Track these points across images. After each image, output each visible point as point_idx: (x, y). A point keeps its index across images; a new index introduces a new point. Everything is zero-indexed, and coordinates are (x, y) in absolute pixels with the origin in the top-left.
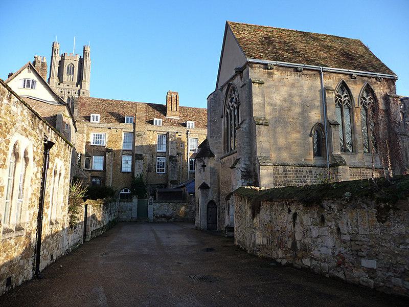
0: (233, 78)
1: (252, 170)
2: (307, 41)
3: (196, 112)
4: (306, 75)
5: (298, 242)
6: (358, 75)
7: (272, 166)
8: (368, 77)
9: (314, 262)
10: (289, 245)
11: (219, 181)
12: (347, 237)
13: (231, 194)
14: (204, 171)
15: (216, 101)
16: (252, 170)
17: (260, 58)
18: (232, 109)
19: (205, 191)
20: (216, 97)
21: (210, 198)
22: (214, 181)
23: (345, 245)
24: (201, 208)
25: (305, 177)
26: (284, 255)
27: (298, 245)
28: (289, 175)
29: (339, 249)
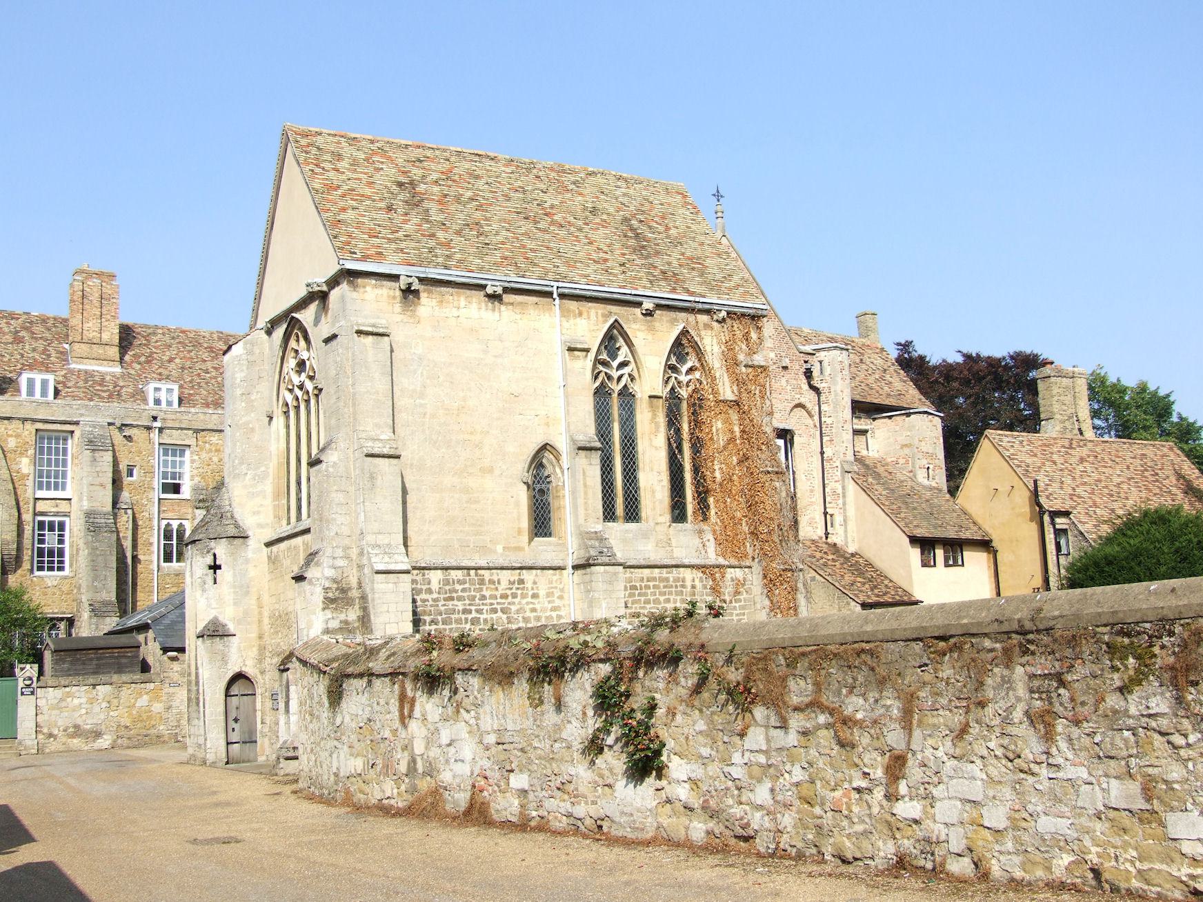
0: (302, 304)
1: (354, 582)
2: (524, 192)
3: (185, 345)
4: (512, 304)
6: (658, 306)
7: (407, 572)
8: (198, 699)
10: (403, 768)
11: (260, 613)
12: (491, 739)
14: (215, 583)
16: (354, 582)
18: (299, 393)
20: (250, 353)
22: (246, 613)
25: (504, 596)
26: (395, 791)
28: (460, 594)
29: (480, 763)
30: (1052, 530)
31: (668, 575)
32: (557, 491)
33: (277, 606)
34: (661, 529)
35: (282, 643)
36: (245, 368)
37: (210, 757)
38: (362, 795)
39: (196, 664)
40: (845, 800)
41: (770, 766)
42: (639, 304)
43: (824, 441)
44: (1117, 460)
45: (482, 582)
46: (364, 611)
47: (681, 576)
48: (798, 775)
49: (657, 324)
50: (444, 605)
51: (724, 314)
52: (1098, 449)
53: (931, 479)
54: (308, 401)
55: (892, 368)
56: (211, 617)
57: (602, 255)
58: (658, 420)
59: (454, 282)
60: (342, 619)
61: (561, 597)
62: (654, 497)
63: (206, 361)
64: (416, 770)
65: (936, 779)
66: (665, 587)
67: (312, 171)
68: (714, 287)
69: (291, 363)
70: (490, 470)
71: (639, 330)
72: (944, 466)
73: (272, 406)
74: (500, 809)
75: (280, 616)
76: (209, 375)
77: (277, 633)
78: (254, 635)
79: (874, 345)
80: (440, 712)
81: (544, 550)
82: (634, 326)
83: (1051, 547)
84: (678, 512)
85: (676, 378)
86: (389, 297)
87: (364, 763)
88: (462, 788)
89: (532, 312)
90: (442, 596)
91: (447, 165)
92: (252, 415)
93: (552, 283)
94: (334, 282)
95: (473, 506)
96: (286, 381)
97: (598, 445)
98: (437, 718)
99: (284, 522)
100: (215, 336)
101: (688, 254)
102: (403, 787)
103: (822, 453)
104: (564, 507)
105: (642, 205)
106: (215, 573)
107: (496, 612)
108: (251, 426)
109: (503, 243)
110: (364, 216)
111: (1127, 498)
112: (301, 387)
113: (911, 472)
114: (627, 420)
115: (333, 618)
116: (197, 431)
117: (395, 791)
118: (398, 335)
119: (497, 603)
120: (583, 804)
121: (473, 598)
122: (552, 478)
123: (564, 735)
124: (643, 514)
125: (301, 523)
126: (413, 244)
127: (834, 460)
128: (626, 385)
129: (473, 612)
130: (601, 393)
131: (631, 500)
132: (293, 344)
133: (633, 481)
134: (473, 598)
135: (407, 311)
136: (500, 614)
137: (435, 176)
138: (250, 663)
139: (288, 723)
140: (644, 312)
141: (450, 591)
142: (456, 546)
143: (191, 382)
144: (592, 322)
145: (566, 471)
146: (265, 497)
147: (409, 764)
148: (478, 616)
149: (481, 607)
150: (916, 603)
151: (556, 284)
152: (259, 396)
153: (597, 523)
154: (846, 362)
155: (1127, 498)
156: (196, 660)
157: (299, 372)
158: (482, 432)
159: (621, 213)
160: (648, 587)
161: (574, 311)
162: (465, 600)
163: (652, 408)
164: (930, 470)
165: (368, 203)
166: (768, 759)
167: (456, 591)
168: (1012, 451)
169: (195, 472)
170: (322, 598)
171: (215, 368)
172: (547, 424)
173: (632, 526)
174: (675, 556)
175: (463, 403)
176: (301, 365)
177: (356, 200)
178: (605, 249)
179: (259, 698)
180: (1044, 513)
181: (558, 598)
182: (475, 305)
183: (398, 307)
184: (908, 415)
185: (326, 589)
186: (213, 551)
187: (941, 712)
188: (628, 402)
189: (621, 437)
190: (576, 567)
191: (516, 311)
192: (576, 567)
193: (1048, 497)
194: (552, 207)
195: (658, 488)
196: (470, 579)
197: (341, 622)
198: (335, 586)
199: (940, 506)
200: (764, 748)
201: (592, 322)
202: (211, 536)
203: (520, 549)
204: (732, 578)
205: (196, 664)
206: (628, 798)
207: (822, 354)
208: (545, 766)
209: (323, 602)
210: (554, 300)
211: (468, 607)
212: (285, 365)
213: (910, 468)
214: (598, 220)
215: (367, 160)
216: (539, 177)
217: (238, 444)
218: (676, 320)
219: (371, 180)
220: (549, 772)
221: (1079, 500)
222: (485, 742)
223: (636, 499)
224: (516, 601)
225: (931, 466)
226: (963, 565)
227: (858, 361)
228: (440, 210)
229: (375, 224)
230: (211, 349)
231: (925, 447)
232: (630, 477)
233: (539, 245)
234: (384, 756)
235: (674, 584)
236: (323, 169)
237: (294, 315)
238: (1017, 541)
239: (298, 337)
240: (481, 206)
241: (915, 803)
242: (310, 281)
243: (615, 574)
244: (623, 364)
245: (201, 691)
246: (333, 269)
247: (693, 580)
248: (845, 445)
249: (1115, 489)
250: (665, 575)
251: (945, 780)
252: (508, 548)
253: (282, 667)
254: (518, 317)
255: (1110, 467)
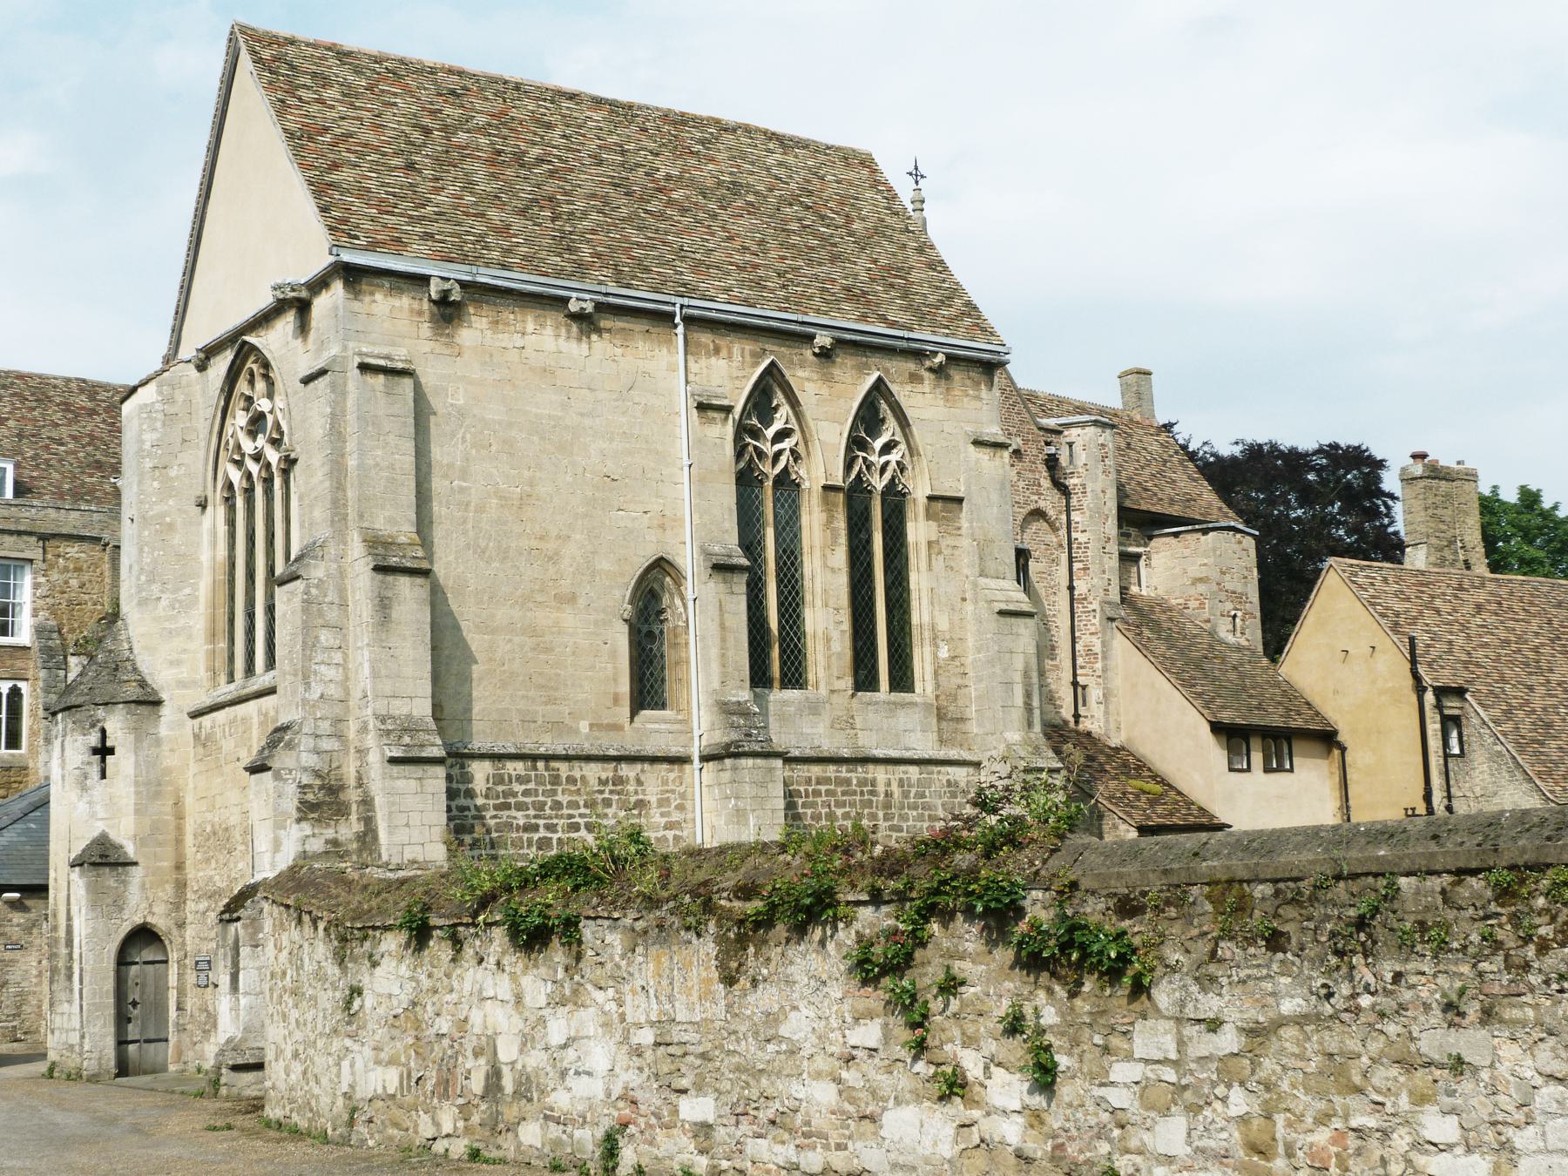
0: (263, 320)
2: (623, 152)
5: (506, 1070)
6: (839, 342)
8: (70, 969)
9: (555, 1131)
10: (477, 1084)
11: (180, 829)
12: (646, 1037)
13: (248, 893)
14: (103, 776)
15: (169, 418)
17: (397, 244)
18: (254, 468)
19: (109, 878)
20: (169, 400)
21: (133, 917)
22: (156, 828)
23: (637, 1061)
24: (86, 967)
26: (461, 1124)
27: (508, 1084)
28: (521, 799)
30: (1438, 718)
31: (849, 775)
32: (676, 636)
33: (209, 816)
34: (841, 701)
35: (217, 877)
36: (159, 424)
37: (89, 1066)
38: (396, 1131)
39: (68, 911)
40: (1334, 1149)
41: (1185, 1087)
42: (811, 337)
43: (1075, 569)
44: (1533, 609)
45: (555, 780)
46: (366, 825)
47: (870, 776)
48: (1239, 1102)
49: (837, 372)
50: (495, 817)
51: (940, 358)
52: (1503, 592)
53: (1238, 634)
54: (268, 481)
55: (1175, 459)
56: (96, 834)
57: (748, 257)
58: (836, 524)
59: (512, 290)
60: (328, 837)
61: (681, 808)
62: (829, 648)
63: (58, 425)
64: (500, 1088)
65: (1519, 1116)
66: (844, 794)
67: (282, 101)
68: (922, 316)
69: (241, 419)
70: (572, 599)
71: (808, 379)
72: (1258, 614)
73: (205, 487)
74: (660, 1156)
75: (214, 834)
76: (63, 448)
77: (208, 861)
78: (167, 864)
79: (1147, 422)
80: (549, 991)
81: (654, 732)
82: (800, 373)
83: (1434, 743)
84: (864, 679)
85: (865, 459)
86: (412, 311)
87: (401, 1076)
88: (588, 1119)
89: (640, 344)
90: (491, 802)
91: (498, 105)
92: (171, 502)
93: (673, 299)
94: (320, 284)
95: (543, 657)
96: (230, 447)
97: (745, 562)
98: (542, 1001)
99: (223, 678)
100: (73, 385)
101: (883, 262)
102: (476, 1119)
103: (1071, 588)
104: (688, 662)
105: (809, 181)
106: (103, 761)
107: (578, 830)
108: (168, 519)
109: (593, 232)
110: (370, 178)
111: (1551, 671)
112: (257, 457)
113: (1208, 621)
114: (787, 523)
115: (314, 835)
116: (44, 538)
117: (461, 1124)
118: (429, 375)
119: (581, 815)
120: (819, 1149)
121: (541, 806)
122: (668, 615)
123: (784, 1030)
124: (811, 677)
125: (253, 679)
126: (449, 228)
127: (1090, 599)
128: (786, 467)
129: (541, 829)
130: (747, 480)
131: (792, 652)
132: (242, 386)
133: (795, 622)
134: (541, 806)
135: (441, 335)
136: (583, 833)
137: (481, 120)
138: (160, 909)
139: (235, 1009)
140: (817, 350)
141: (506, 794)
142: (515, 721)
143: (34, 458)
144: (735, 364)
145: (690, 604)
146: (190, 637)
147: (487, 1077)
148: (549, 835)
149: (555, 821)
150: (1222, 827)
151: (679, 301)
152: (182, 472)
153: (741, 687)
154: (1111, 445)
155: (1551, 671)
156: (69, 904)
157: (253, 434)
158: (559, 537)
159: (777, 193)
160: (817, 793)
161: (706, 346)
162: (528, 809)
163: (828, 506)
164: (1238, 620)
165: (374, 157)
166: (1181, 1076)
167: (515, 795)
168: (1372, 591)
169: (41, 602)
170: (296, 802)
171: (74, 438)
172: (662, 527)
173: (793, 694)
174: (860, 744)
175: (527, 488)
176: (257, 423)
177: (355, 152)
178: (754, 248)
179: (173, 970)
180: (1425, 689)
181: (677, 807)
182: (549, 331)
183: (426, 329)
184: (1205, 532)
185: (303, 788)
186: (100, 725)
187: (1528, 999)
188: (789, 495)
189: (777, 551)
190: (705, 759)
191: (615, 341)
192: (705, 759)
193: (1430, 665)
194: (668, 177)
195: (835, 635)
196: (536, 775)
197: (327, 842)
198: (318, 782)
199: (1254, 676)
200: (1173, 1056)
201: (735, 364)
202: (98, 700)
203: (617, 727)
204: (948, 781)
205: (68, 911)
206: (907, 1140)
207: (1074, 431)
208: (747, 1083)
209: (299, 809)
210: (676, 326)
211: (533, 821)
212: (229, 421)
213: (1206, 616)
214: (740, 203)
215: (370, 88)
216: (646, 130)
217: (146, 549)
218: (867, 366)
219: (378, 121)
220: (755, 1094)
221: (1479, 671)
222: (635, 1040)
223: (800, 651)
224: (610, 811)
225: (1239, 614)
226: (1291, 770)
227: (1123, 445)
228: (492, 175)
229: (387, 193)
230: (66, 407)
231: (1231, 584)
232: (791, 616)
233: (650, 238)
234: (440, 1065)
235: (858, 789)
236: (300, 99)
237: (247, 338)
238: (1379, 732)
239: (252, 374)
240: (556, 171)
241: (1476, 1157)
242: (279, 281)
243: (771, 770)
244: (782, 435)
245: (76, 956)
246: (321, 261)
247: (889, 784)
248: (1106, 576)
249: (1531, 655)
250: (844, 775)
251: (1539, 1119)
252: (597, 725)
253: (227, 916)
254: (619, 351)
255: (1523, 620)
